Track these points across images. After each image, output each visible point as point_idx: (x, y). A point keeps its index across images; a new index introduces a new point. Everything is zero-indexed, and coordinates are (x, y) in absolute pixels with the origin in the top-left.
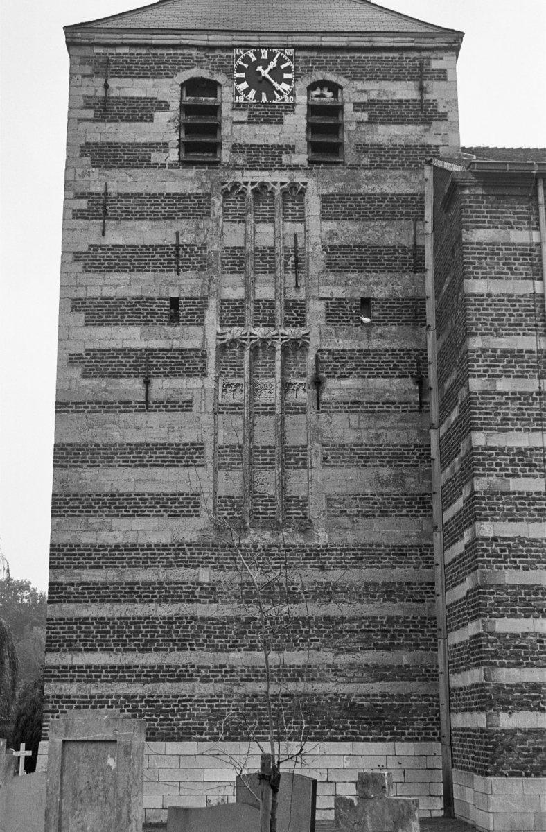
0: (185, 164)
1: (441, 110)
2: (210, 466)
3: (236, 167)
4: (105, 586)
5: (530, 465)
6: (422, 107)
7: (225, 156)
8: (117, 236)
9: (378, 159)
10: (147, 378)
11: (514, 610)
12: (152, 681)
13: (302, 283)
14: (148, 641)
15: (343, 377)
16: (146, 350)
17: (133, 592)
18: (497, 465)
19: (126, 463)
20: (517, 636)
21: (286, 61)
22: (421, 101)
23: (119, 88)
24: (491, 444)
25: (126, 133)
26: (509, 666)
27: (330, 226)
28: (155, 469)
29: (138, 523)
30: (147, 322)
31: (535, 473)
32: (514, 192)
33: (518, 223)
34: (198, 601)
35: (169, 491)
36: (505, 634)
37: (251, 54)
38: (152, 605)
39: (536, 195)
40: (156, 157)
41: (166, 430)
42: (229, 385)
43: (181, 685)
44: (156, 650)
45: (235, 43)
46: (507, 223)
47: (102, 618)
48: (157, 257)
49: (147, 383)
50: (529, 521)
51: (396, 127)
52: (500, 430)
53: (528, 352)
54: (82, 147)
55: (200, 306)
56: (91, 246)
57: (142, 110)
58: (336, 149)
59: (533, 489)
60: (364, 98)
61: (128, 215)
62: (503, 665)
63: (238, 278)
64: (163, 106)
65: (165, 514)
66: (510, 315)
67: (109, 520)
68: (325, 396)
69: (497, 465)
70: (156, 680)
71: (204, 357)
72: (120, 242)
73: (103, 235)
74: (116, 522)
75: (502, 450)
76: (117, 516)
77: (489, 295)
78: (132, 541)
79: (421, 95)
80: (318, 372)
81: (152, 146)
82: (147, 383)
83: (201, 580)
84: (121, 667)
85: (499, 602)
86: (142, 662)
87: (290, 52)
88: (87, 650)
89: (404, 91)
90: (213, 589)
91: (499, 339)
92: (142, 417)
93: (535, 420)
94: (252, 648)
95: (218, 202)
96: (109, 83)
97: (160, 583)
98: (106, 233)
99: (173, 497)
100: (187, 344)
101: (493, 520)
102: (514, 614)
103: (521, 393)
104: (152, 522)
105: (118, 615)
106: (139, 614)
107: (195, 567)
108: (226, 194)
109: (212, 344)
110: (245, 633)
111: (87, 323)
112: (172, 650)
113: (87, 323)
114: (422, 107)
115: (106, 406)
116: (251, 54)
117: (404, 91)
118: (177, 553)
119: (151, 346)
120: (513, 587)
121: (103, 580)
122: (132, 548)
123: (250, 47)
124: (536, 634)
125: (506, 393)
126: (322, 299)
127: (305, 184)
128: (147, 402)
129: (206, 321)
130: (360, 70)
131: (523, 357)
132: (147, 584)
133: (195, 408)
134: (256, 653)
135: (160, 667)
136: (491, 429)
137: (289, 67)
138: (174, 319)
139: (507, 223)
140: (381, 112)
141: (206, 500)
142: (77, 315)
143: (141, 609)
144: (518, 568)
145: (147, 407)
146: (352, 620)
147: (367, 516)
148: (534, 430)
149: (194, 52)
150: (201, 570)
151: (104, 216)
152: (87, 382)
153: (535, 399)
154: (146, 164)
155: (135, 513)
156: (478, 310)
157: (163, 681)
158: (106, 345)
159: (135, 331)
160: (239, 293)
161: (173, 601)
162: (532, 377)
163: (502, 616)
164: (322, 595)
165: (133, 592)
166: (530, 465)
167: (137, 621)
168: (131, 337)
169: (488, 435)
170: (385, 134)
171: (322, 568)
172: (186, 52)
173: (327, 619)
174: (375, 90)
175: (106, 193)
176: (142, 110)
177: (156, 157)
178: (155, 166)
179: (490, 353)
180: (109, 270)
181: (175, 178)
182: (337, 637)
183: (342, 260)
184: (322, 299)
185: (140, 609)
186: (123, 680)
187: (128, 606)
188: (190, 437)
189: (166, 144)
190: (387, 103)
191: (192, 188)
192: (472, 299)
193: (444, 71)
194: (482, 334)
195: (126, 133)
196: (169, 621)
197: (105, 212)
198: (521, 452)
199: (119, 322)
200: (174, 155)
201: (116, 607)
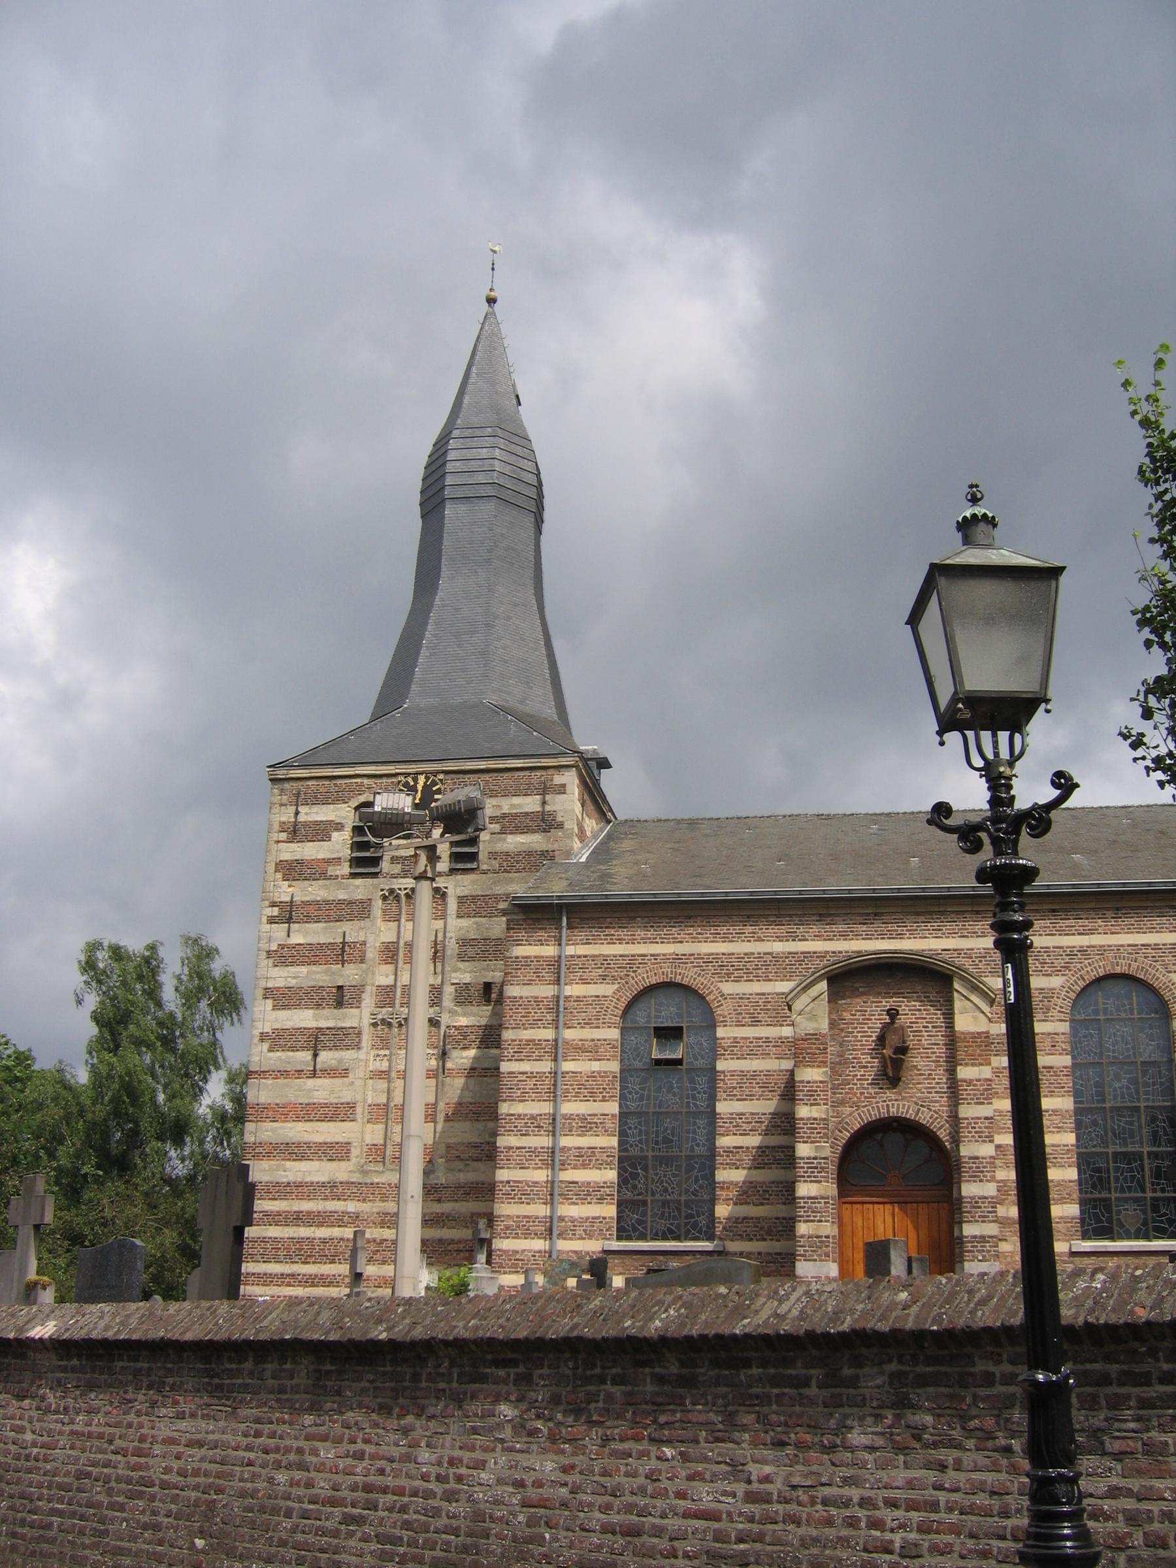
0: (354, 875)
1: (559, 819)
2: (359, 1120)
3: (394, 876)
4: (279, 1214)
5: (539, 1127)
6: (543, 818)
7: (385, 865)
8: (301, 935)
9: (505, 864)
10: (315, 1051)
11: (517, 1234)
12: (310, 1286)
13: (439, 969)
14: (309, 1256)
15: (465, 1048)
16: (317, 1028)
17: (298, 1218)
18: (515, 1127)
19: (298, 1119)
20: (517, 1252)
21: (437, 784)
22: (543, 812)
23: (306, 814)
24: (511, 1112)
25: (310, 851)
26: (510, 1273)
27: (465, 923)
28: (319, 1123)
29: (304, 1166)
30: (318, 1006)
31: (542, 1133)
32: (547, 916)
33: (548, 941)
34: (346, 1226)
35: (328, 1140)
36: (508, 1251)
37: (410, 780)
38: (312, 1229)
39: (561, 919)
40: (331, 871)
41: (328, 1092)
42: (378, 1056)
43: (331, 1289)
44: (314, 1263)
45: (398, 771)
46: (539, 941)
47: (276, 1238)
48: (329, 953)
49: (315, 1055)
50: (534, 1168)
51: (523, 836)
52: (519, 1101)
53: (545, 1041)
54: (276, 864)
55: (360, 989)
56: (279, 945)
57: (321, 832)
58: (473, 857)
59: (539, 1145)
60: (498, 813)
61: (308, 919)
62: (505, 1273)
63: (391, 968)
64: (339, 827)
65: (325, 1159)
66: (535, 1013)
67: (283, 1162)
68: (449, 1065)
69: (515, 1127)
70: (313, 1285)
71: (359, 1034)
72: (301, 942)
73: (289, 936)
74: (289, 1164)
75: (519, 1115)
76: (289, 1160)
77: (521, 998)
78: (299, 1180)
79: (543, 808)
80: (444, 1044)
81: (329, 861)
82: (315, 1055)
83: (349, 1210)
84: (288, 1275)
85: (507, 1228)
86: (303, 1271)
87: (441, 776)
88: (264, 1262)
89: (530, 804)
90: (357, 1217)
91: (525, 1032)
92: (311, 1083)
93: (546, 1093)
94: (384, 1262)
95: (378, 904)
96: (299, 809)
97: (319, 1212)
98: (291, 934)
99: (331, 1145)
100: (347, 1024)
101: (508, 1168)
102: (517, 1237)
103: (537, 1073)
104: (315, 1165)
105: (287, 1236)
106: (302, 1236)
107: (345, 1200)
108: (385, 898)
109: (366, 1021)
110: (378, 1251)
111: (275, 1008)
112: (325, 1263)
113: (275, 1008)
114: (543, 818)
115: (284, 1074)
116: (410, 780)
117: (530, 804)
118: (332, 1189)
119: (320, 1025)
120: (518, 1217)
121: (278, 1209)
122: (299, 1185)
123: (409, 774)
124: (530, 1251)
125: (526, 1073)
126: (453, 984)
127: (446, 888)
128: (315, 1070)
129: (363, 1005)
130: (496, 788)
131: (541, 1045)
132: (309, 1213)
133: (351, 1075)
134: (386, 1267)
135: (316, 1276)
136: (512, 1100)
137: (439, 789)
138: (339, 1003)
139: (539, 941)
140: (513, 823)
141: (355, 1147)
142: (267, 1001)
143: (304, 1232)
144: (523, 1203)
145: (315, 1074)
146: (460, 1242)
147: (478, 1160)
148: (544, 1101)
149: (366, 781)
150: (349, 1202)
151: (289, 920)
152: (271, 1054)
153: (547, 1077)
154: (324, 876)
155: (302, 1157)
156: (511, 1009)
157: (318, 1286)
158: (288, 1025)
159: (309, 1013)
160: (389, 981)
161: (327, 1226)
162: (546, 1060)
163: (508, 1238)
164: (438, 1222)
165: (298, 1218)
166: (539, 1127)
167: (300, 1241)
168: (305, 1018)
169: (511, 1105)
170: (515, 842)
171: (439, 1201)
172: (359, 780)
173: (441, 1241)
174: (508, 805)
175: (292, 902)
176: (321, 832)
177: (331, 871)
178: (330, 878)
179: (518, 1042)
180: (292, 964)
181: (346, 887)
182: (446, 1255)
183: (471, 951)
184: (453, 984)
185: (304, 1232)
186: (289, 1285)
187: (295, 1228)
188: (347, 1097)
189: (340, 859)
190: (516, 815)
191: (359, 895)
192: (508, 1001)
193: (564, 786)
194: (513, 1028)
195: (310, 851)
196: (324, 1241)
197: (291, 918)
198: (533, 1117)
199: (298, 1006)
200: (346, 869)
201: (287, 1229)
